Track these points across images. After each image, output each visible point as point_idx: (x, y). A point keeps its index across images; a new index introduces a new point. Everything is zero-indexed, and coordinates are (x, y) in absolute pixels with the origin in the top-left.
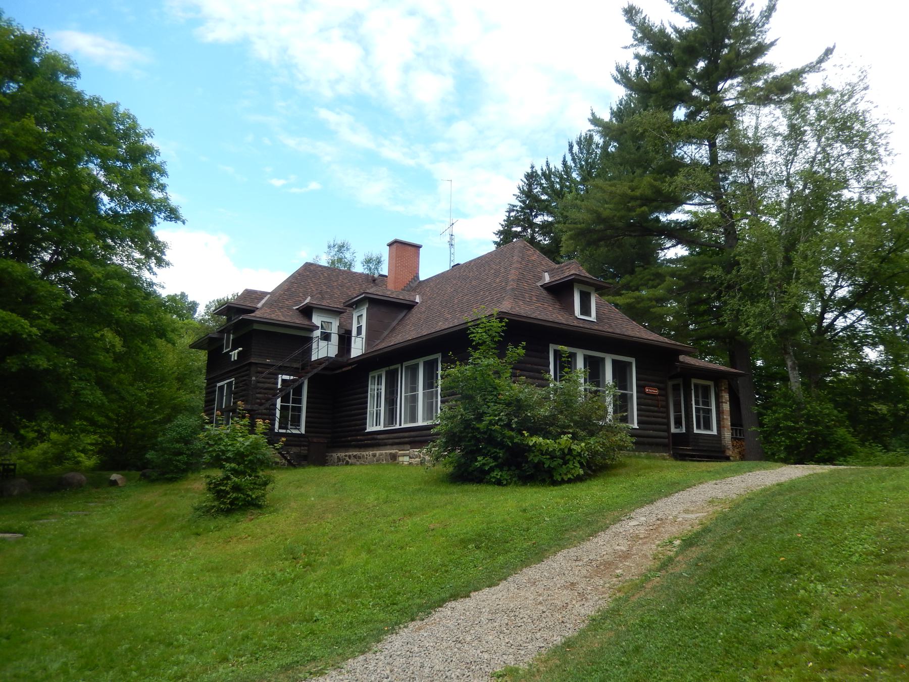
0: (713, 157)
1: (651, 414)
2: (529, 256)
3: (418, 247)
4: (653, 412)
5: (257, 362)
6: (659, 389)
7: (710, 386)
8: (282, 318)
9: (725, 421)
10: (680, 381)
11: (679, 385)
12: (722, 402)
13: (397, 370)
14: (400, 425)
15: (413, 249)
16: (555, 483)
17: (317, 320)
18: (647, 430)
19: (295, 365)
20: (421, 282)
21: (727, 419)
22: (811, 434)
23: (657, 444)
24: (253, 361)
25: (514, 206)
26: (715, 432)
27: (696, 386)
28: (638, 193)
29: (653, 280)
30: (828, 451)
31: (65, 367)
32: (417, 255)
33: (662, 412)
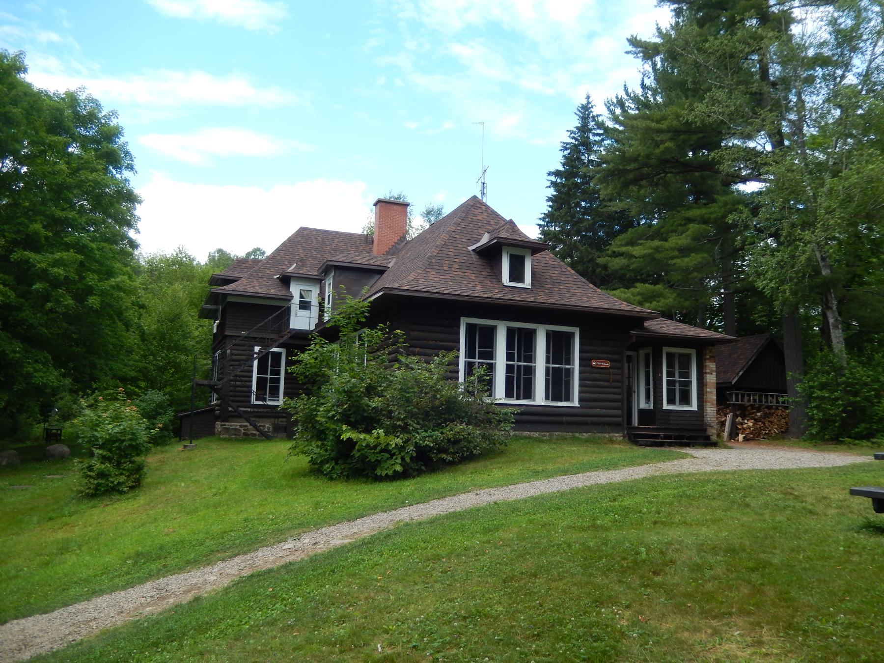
1: (600, 390)
2: (475, 215)
3: (406, 205)
4: (605, 387)
5: (231, 334)
6: (611, 360)
8: (257, 289)
10: (649, 350)
12: (706, 373)
15: (399, 208)
16: (378, 479)
17: (295, 289)
18: (596, 408)
20: (408, 242)
21: (711, 393)
22: (845, 406)
23: (609, 424)
25: (567, 144)
28: (664, 125)
30: (868, 426)
31: (15, 352)
32: (405, 214)
33: (615, 388)
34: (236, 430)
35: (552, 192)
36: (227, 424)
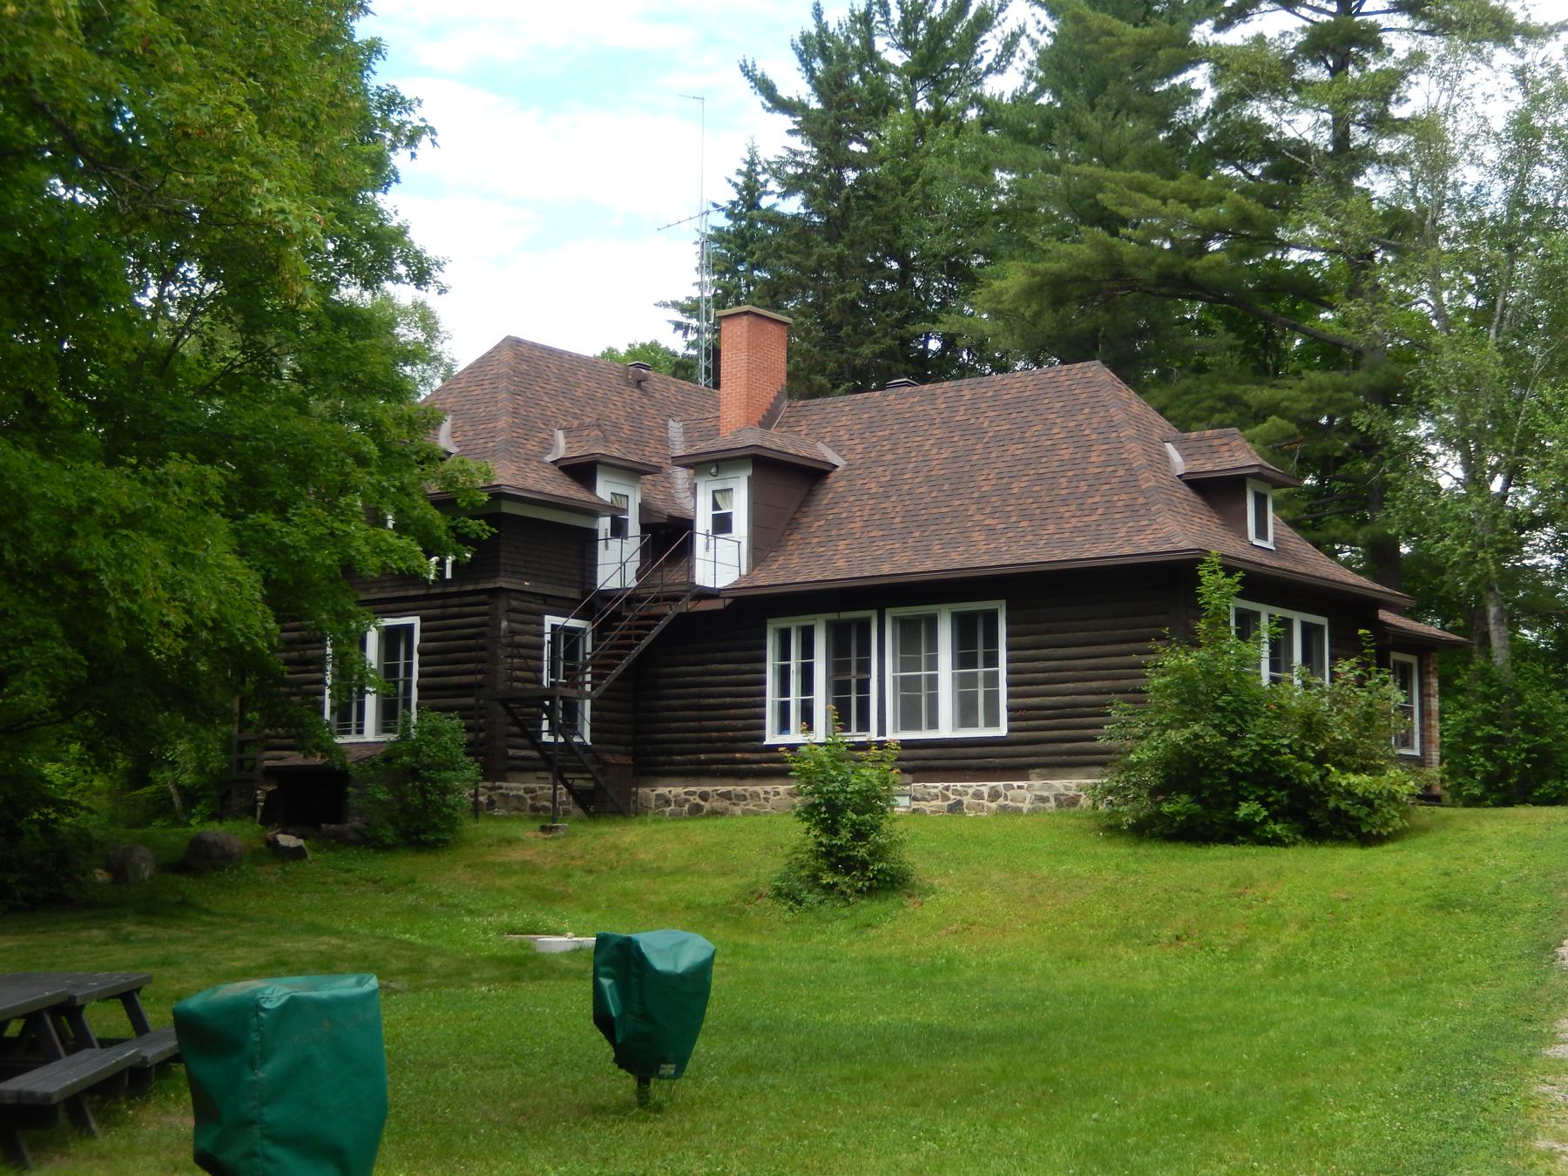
0: (1341, 140)
7: (1411, 664)
10: (794, 624)
13: (864, 627)
14: (882, 731)
17: (605, 489)
24: (504, 585)
29: (1221, 411)
34: (518, 797)
35: (380, 77)
36: (505, 784)
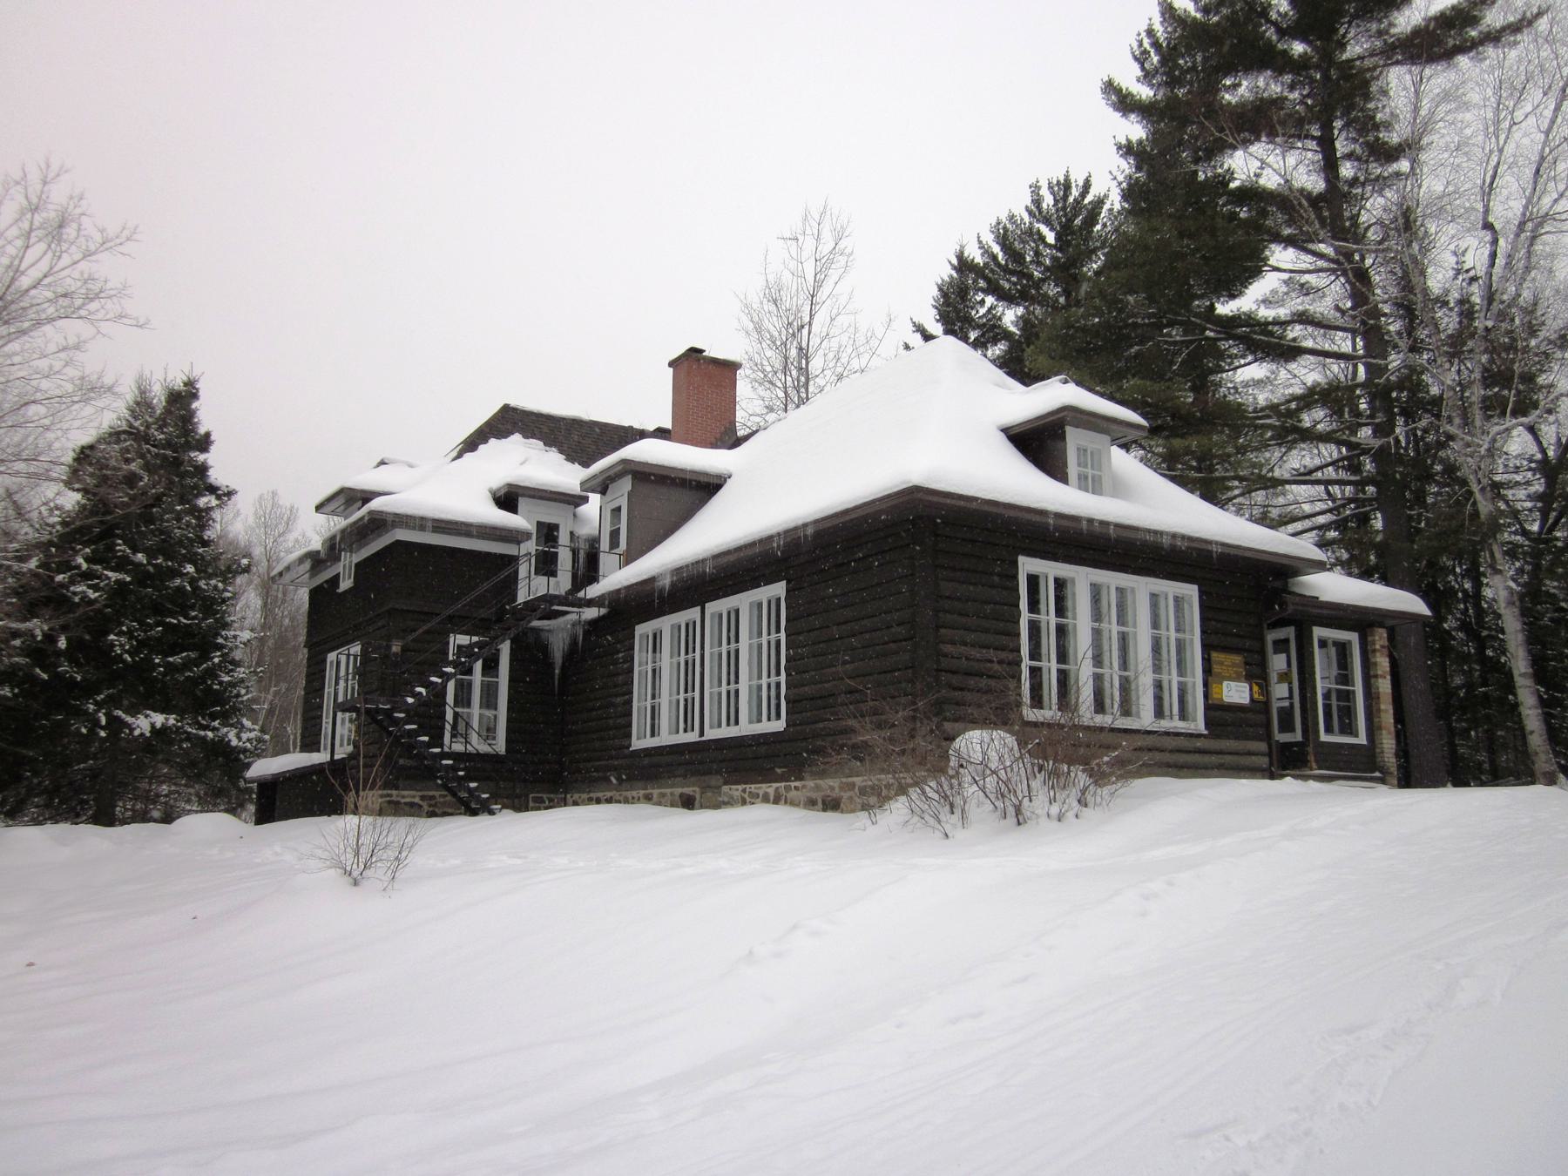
7: (1350, 642)
9: (1382, 715)
10: (1289, 632)
11: (1287, 641)
12: (1376, 676)
14: (702, 734)
19: (483, 613)
21: (1386, 711)
26: (1362, 739)
27: (1323, 643)
